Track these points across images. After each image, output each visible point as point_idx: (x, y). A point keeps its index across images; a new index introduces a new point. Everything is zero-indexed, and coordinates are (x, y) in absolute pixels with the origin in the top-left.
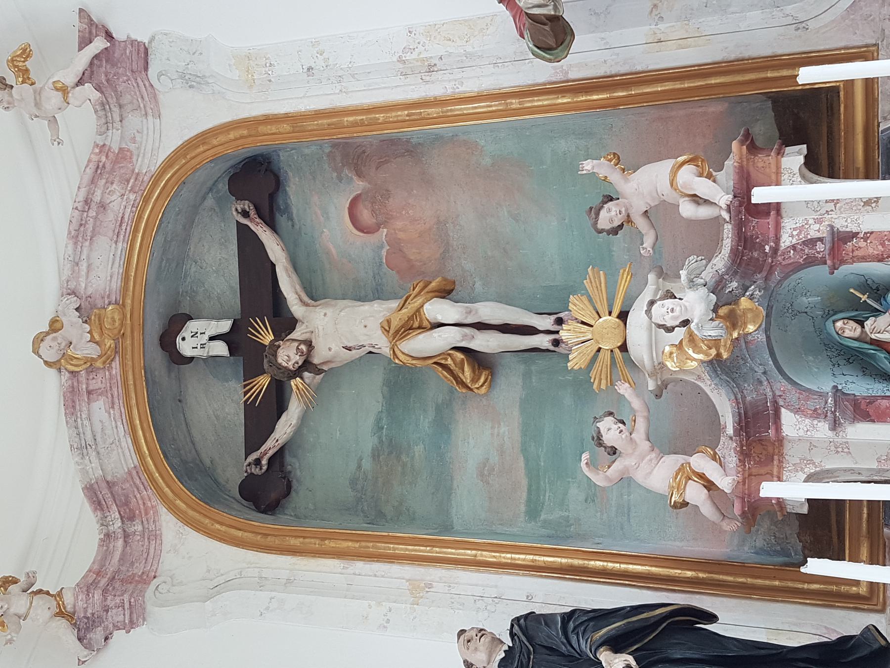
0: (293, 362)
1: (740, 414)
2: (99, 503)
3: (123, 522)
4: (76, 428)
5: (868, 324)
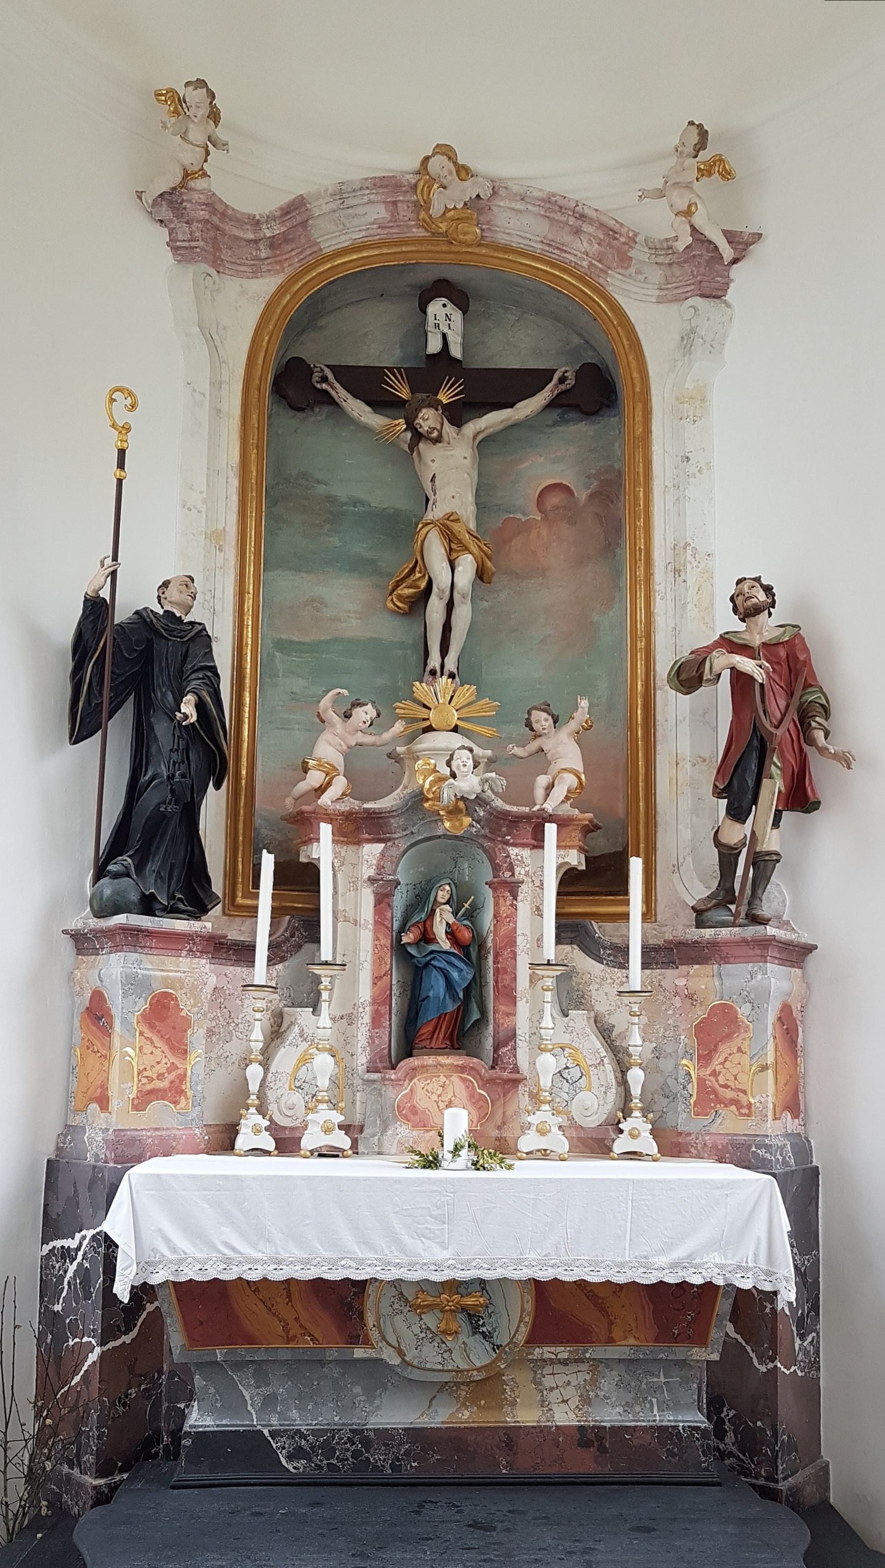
0: (423, 424)
1: (381, 813)
2: (288, 213)
3: (269, 238)
4: (361, 189)
5: (448, 907)
